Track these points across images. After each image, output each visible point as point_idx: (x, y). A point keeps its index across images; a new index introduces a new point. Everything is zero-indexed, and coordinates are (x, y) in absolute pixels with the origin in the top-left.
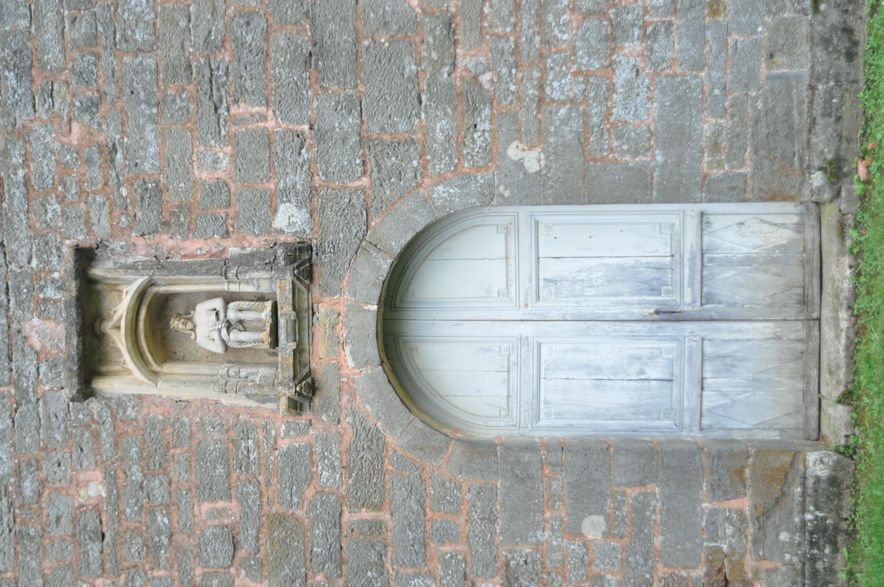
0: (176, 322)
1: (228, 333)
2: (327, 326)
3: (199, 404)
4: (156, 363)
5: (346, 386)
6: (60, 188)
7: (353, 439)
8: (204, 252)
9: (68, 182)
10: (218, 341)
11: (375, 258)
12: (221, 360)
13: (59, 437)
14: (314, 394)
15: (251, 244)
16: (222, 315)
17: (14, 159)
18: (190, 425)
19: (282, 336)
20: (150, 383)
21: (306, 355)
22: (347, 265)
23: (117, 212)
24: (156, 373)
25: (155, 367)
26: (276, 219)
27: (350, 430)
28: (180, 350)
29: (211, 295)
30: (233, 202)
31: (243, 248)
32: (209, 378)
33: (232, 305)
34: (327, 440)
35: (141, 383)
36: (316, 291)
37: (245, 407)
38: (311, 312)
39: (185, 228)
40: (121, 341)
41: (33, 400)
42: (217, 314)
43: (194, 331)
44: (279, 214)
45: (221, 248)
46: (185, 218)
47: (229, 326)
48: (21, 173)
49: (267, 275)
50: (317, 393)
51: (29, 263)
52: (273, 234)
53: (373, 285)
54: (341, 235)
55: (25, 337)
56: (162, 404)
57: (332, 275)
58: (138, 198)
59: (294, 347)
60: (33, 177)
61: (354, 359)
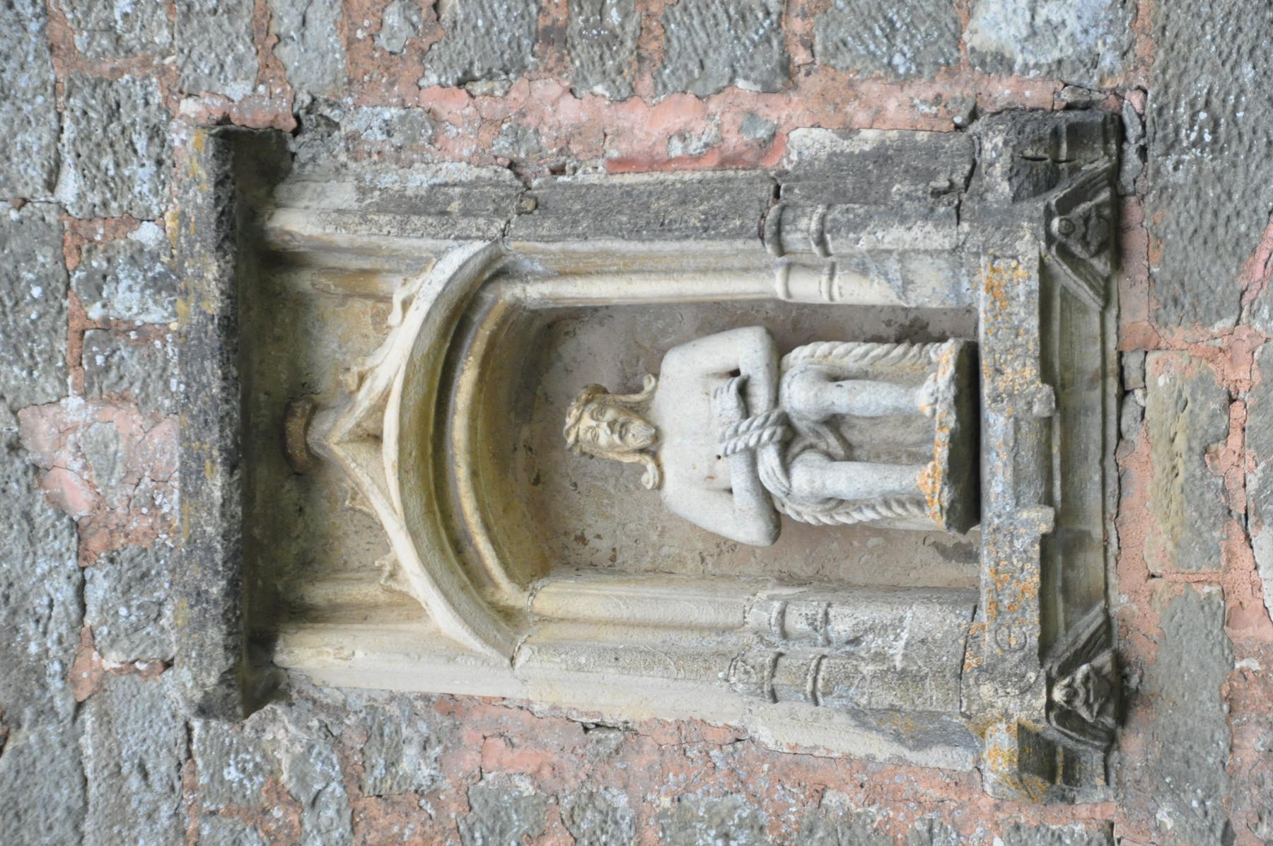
0: (587, 421)
1: (786, 467)
2: (1180, 443)
3: (669, 740)
4: (510, 575)
8: (695, 146)
10: (744, 498)
12: (753, 569)
15: (877, 116)
16: (760, 396)
18: (636, 825)
20: (488, 651)
24: (508, 615)
25: (508, 592)
28: (601, 526)
29: (720, 317)
31: (848, 131)
32: (711, 642)
33: (799, 356)
35: (454, 653)
36: (1136, 301)
38: (1113, 387)
40: (384, 492)
41: (64, 706)
42: (743, 391)
43: (655, 456)
45: (762, 133)
47: (789, 440)
49: (940, 238)
50: (1138, 716)
51: (51, 186)
52: (966, 74)
54: (1247, 71)
55: (36, 468)
56: (530, 736)
59: (1045, 528)
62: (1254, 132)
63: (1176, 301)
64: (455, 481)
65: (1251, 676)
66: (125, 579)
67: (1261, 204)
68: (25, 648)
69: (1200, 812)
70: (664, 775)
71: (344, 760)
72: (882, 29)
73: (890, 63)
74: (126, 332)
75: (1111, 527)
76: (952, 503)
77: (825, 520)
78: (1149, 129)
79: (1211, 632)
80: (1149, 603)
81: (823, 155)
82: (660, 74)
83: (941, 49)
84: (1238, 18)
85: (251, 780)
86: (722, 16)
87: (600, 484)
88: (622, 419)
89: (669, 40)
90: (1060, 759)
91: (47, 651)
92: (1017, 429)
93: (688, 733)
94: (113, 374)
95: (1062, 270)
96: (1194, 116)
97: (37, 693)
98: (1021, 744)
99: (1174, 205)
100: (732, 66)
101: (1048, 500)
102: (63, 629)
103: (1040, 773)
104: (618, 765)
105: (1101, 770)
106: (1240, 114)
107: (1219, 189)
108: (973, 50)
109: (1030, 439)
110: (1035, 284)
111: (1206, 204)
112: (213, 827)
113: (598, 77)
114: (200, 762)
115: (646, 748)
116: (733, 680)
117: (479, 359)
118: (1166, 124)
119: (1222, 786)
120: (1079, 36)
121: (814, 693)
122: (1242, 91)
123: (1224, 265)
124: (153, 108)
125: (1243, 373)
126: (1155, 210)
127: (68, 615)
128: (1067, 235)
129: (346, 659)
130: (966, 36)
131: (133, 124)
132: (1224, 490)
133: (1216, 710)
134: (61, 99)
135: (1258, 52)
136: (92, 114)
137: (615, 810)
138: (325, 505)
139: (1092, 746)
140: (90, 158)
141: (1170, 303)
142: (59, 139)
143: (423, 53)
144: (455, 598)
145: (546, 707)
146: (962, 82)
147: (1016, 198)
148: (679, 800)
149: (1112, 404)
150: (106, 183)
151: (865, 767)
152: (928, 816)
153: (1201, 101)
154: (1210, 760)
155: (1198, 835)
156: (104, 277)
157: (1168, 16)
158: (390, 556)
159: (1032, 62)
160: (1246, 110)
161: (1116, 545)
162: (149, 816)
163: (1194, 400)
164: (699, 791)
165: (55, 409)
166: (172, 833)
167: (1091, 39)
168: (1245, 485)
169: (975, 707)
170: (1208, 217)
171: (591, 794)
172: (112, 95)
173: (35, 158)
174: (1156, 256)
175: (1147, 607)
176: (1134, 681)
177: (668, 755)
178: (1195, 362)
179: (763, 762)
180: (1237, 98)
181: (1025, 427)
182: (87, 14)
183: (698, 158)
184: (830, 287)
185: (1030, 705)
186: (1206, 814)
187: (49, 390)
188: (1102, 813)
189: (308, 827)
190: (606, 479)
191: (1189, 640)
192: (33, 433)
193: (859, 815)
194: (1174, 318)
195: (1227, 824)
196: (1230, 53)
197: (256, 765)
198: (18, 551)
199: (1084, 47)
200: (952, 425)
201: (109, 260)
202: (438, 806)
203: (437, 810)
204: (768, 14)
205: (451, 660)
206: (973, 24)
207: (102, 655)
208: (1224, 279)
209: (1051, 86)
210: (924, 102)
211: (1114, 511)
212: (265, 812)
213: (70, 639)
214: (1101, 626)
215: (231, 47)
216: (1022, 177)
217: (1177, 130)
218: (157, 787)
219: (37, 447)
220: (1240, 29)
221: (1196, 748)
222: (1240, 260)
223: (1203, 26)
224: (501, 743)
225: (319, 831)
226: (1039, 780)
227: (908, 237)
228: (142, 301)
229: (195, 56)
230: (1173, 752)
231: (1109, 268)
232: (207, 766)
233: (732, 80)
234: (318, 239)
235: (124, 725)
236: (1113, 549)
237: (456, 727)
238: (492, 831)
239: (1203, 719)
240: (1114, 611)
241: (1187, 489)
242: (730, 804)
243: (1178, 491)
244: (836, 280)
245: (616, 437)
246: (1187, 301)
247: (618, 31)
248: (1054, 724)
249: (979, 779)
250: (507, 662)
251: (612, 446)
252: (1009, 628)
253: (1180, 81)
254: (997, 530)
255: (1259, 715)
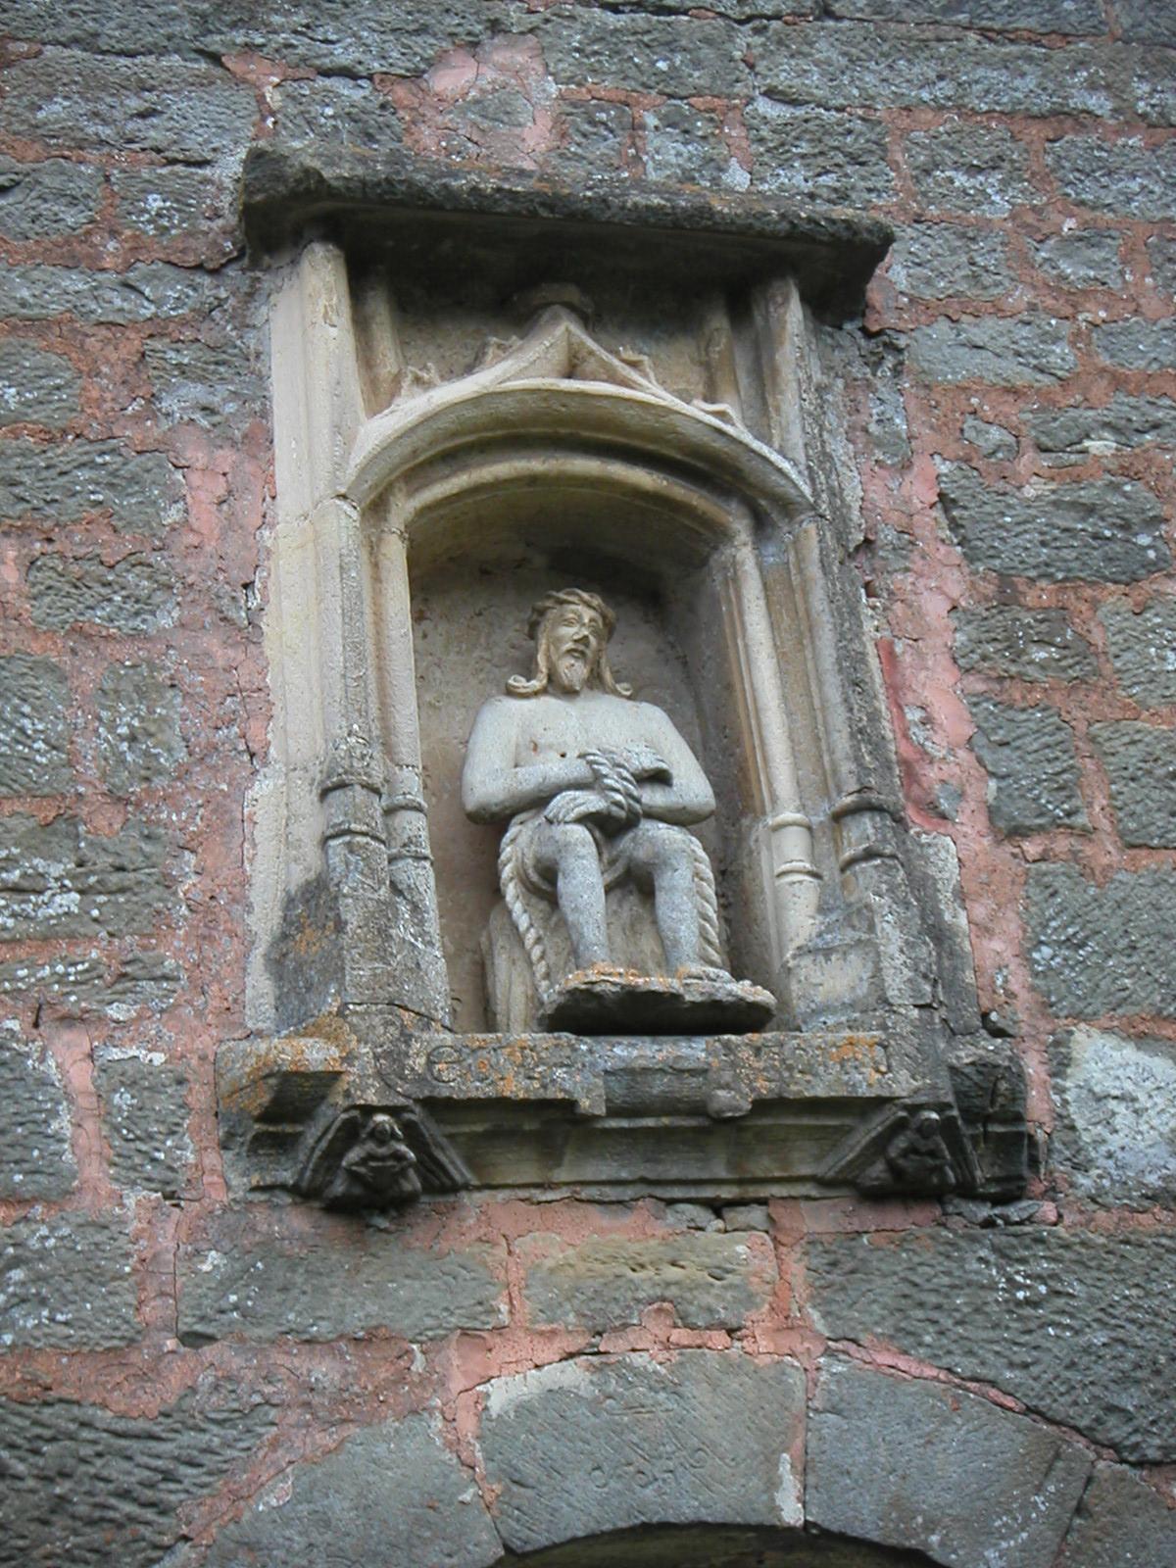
0: (588, 615)
1: (582, 820)
2: (673, 1273)
3: (243, 677)
5: (383, 1373)
6: (1069, 224)
7: (103, 1417)
8: (919, 734)
9: (1098, 255)
10: (531, 777)
11: (1027, 1506)
13: (55, 110)
14: (337, 1208)
15: (984, 930)
16: (654, 797)
17: (1146, 88)
18: (136, 635)
19: (626, 1051)
21: (530, 1173)
22: (965, 1365)
23: (1021, 413)
25: (404, 508)
26: (1111, 1041)
27: (152, 1399)
30: (1147, 861)
31: (961, 896)
34: (96, 1277)
36: (823, 1219)
37: (246, 882)
38: (726, 1193)
39: (1003, 665)
40: (520, 374)
41: (214, 43)
43: (544, 691)
44: (1130, 1052)
45: (944, 805)
46: (1043, 666)
48: (1099, 103)
49: (896, 984)
50: (335, 1228)
51: (771, 93)
52: (1044, 1025)
53: (896, 1503)
54: (1100, 1338)
55: (475, 45)
56: (232, 524)
57: (910, 1296)
58: (1085, 496)
59: (585, 1104)
60: (1093, 139)
61: (524, 1409)
62: (1036, 1348)
63: (834, 1264)
64: (529, 459)
65: (402, 1363)
66: (365, 117)
67: (957, 1359)
68: (276, 12)
69: (223, 1304)
70: (201, 670)
71: (184, 322)
72: (1075, 934)
73: (1042, 943)
74: (634, 145)
75: (565, 1192)
76: (599, 996)
77: (507, 872)
78: (1017, 1229)
79: (452, 1314)
80: (480, 1240)
81: (932, 871)
82: (987, 700)
83: (1064, 998)
84: (1153, 1324)
85: (149, 222)
86: (1058, 767)
87: (482, 640)
88: (588, 652)
89: (1023, 710)
90: (289, 1129)
91: (275, 32)
92: (693, 1072)
93: (254, 699)
94: (586, 127)
95: (877, 1125)
96: (1040, 1278)
97: (227, 18)
98: (316, 1075)
99: (941, 1259)
100: (1008, 776)
101: (614, 1112)
102: (301, 50)
103: (275, 1101)
104: (208, 619)
105: (269, 1180)
106: (1051, 1331)
107: (966, 1310)
108: (1071, 1033)
109: (689, 1088)
110: (863, 1091)
111: (947, 1296)
112: (91, 177)
113: (974, 635)
114: (164, 171)
115: (231, 653)
116: (352, 740)
117: (665, 492)
118: (1027, 1248)
119: (259, 1332)
120: (1103, 1149)
121: (349, 832)
122: (1077, 1332)
123: (883, 1318)
124: (866, 196)
125: (764, 1344)
126: (932, 1238)
127: (318, 57)
128: (919, 1130)
129: (326, 316)
130: (1082, 1025)
131: (846, 175)
132: (625, 1326)
133: (355, 1322)
134: (860, 112)
135: (1120, 1348)
136: (849, 139)
137: (153, 613)
138: (471, 328)
139: (304, 1169)
140: (805, 131)
141: (832, 1257)
142: (819, 106)
143: (967, 460)
144: (406, 441)
145: (269, 544)
146: (1034, 1022)
147: (953, 1069)
148: (173, 686)
149: (708, 1192)
150: (782, 144)
151: (234, 900)
152: (184, 975)
153: (1059, 1287)
154: (291, 1316)
155: (193, 1303)
156: (686, 132)
157: (1141, 1246)
158: (437, 380)
159: (1067, 1097)
160: (1058, 1337)
161: (543, 1198)
162: (96, 114)
163: (725, 1288)
164: (185, 709)
165: (540, 69)
166: (80, 135)
167: (1102, 1162)
168: (634, 1350)
169: (355, 1020)
170: (933, 1299)
171: (170, 587)
172: (874, 159)
173: (797, 81)
174: (880, 1239)
175: (474, 1236)
176: (383, 1223)
177: (223, 676)
178: (768, 1288)
179: (229, 784)
180: (1068, 1327)
181: (695, 1081)
182: (945, 145)
183: (906, 736)
184: (799, 872)
185: (368, 1087)
186: (222, 1312)
187: (561, 66)
188: (211, 1184)
189: (100, 276)
190: (488, 648)
191: (438, 1289)
192: (510, 46)
193: (175, 893)
194: (815, 1262)
195: (210, 1339)
196: (1114, 1317)
197: (167, 229)
198: (385, 16)
199: (1093, 1154)
200: (688, 998)
201: (704, 138)
202: (137, 418)
203: (131, 417)
204: (1069, 814)
205: (337, 429)
206: (1095, 1032)
207: (278, 85)
208: (866, 1318)
209: (1046, 1119)
210: (1006, 981)
211: (583, 1196)
212: (114, 233)
213: (292, 56)
214: (451, 1178)
215: (942, 275)
216: (976, 1078)
217: (1023, 1261)
218: (131, 125)
219: (497, 48)
220: (1142, 1327)
221: (304, 1299)
222: (892, 1337)
223: (1137, 1286)
224: (221, 491)
225: (96, 288)
226: (265, 1098)
227: (893, 949)
228: (667, 165)
229: (926, 240)
230: (294, 1271)
231: (869, 1183)
232: (161, 177)
233: (992, 775)
234: (784, 328)
235: (201, 99)
236: (539, 1195)
237: (234, 444)
238: (114, 474)
239: (342, 1306)
240: (465, 1198)
241: (619, 1282)
242: (174, 744)
243: (617, 1271)
244: (808, 878)
245: (570, 645)
246: (835, 1277)
247: (1025, 658)
248: (344, 1116)
249: (236, 1035)
250: (343, 490)
251: (558, 641)
252: (458, 1062)
253: (1076, 1262)
254: (574, 1050)
255: (355, 1375)
